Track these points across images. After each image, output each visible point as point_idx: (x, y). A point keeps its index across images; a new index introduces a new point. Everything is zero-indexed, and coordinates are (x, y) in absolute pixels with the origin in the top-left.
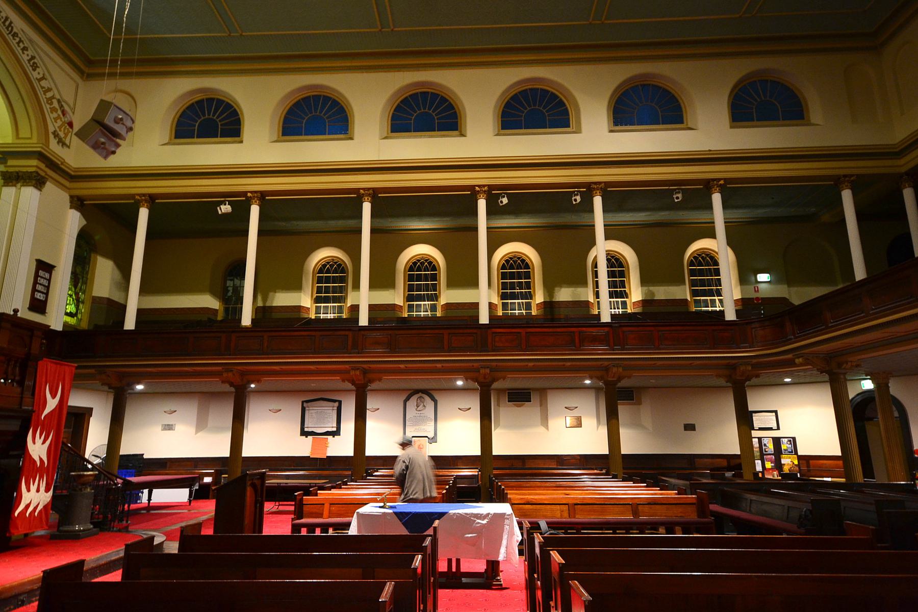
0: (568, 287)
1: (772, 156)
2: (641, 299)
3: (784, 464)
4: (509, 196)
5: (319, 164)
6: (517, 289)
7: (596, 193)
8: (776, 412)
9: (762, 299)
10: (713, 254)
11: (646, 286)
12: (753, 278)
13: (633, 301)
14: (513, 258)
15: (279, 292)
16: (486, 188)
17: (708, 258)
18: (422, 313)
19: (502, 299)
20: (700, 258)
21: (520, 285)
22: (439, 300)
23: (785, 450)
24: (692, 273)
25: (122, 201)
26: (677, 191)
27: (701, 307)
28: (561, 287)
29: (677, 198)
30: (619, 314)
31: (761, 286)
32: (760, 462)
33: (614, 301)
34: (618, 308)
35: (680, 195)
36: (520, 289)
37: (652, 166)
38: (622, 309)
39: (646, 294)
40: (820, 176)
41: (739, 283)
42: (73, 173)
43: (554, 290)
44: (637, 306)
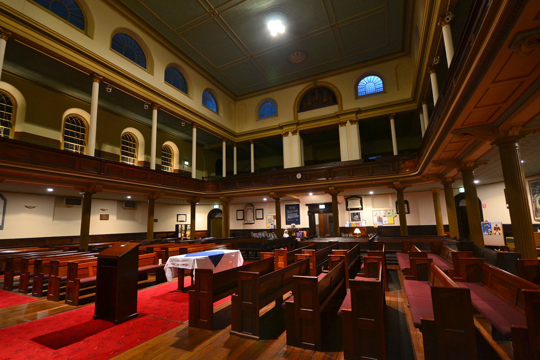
0: (110, 145)
1: (31, 25)
2: (143, 160)
3: (187, 234)
4: (113, 88)
5: (31, 20)
6: (76, 137)
7: (96, 80)
8: (186, 215)
9: (185, 171)
10: (9, 96)
11: (147, 155)
12: (183, 163)
13: (138, 160)
14: (75, 118)
15: (108, 145)
16: (197, 125)
17: (79, 121)
18: (74, 151)
19: (64, 140)
20: (74, 119)
21: (78, 135)
22: (13, 127)
23: (188, 229)
24: (67, 126)
25: (136, 97)
26: (146, 103)
27: (124, 161)
28: (106, 144)
29: (183, 124)
30: (131, 165)
31: (185, 166)
32: (180, 234)
33: (129, 158)
34: (131, 162)
35: (111, 89)
36: (78, 138)
37: (142, 88)
38: (75, 150)
39: (146, 159)
40: (208, 129)
41: (144, 154)
43: (102, 144)
44: (140, 163)
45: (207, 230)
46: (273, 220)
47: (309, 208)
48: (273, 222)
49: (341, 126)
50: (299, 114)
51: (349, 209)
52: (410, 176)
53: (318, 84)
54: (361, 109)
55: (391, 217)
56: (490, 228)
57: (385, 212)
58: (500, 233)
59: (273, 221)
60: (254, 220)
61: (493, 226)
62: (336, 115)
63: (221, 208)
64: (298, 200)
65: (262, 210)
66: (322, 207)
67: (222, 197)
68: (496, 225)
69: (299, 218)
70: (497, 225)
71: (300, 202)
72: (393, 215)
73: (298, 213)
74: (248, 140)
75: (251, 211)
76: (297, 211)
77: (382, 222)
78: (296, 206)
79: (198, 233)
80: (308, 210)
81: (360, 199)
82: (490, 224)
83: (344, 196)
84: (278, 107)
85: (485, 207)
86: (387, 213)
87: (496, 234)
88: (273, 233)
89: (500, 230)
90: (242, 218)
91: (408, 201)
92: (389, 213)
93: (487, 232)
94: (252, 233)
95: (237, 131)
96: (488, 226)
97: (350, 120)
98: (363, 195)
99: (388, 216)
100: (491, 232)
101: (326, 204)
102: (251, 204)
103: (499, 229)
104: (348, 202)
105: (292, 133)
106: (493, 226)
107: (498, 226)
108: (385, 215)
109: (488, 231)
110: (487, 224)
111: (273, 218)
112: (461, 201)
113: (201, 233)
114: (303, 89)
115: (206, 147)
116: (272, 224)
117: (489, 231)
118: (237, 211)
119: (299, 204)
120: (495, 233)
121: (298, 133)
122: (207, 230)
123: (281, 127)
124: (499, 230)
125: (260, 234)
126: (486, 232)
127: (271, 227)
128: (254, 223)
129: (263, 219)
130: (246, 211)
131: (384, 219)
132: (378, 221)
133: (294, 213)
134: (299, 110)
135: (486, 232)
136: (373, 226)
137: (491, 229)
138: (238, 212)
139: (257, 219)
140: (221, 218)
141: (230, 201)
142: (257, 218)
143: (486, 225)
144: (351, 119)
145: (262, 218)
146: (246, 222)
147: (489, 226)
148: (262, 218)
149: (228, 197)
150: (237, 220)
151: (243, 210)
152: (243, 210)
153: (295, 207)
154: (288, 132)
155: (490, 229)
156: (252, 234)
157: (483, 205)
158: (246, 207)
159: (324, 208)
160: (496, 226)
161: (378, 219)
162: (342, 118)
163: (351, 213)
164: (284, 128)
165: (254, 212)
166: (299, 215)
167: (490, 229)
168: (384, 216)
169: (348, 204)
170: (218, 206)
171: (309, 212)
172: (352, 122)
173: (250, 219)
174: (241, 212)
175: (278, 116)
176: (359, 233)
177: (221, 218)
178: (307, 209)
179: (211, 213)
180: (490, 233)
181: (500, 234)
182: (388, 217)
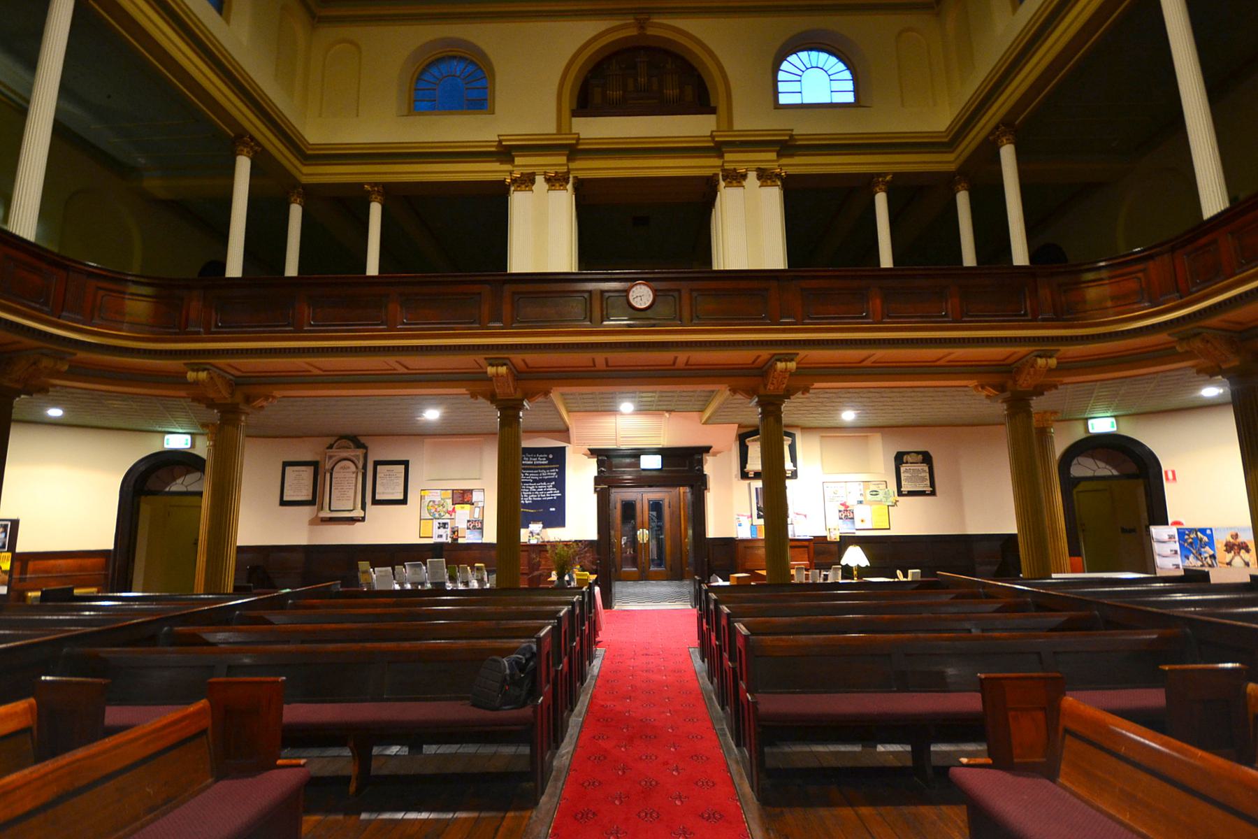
42: (946, 140)
45: (111, 546)
46: (450, 508)
47: (600, 464)
48: (447, 516)
49: (729, 185)
50: (574, 119)
51: (751, 475)
52: (1122, 332)
53: (651, 31)
54: (796, 140)
55: (883, 507)
56: (1211, 543)
57: (861, 487)
58: (1247, 560)
59: (449, 512)
60: (363, 508)
61: (1221, 539)
62: (712, 144)
63: (203, 449)
64: (564, 433)
65: (402, 467)
66: (651, 462)
67: (203, 375)
68: (1236, 536)
69: (560, 503)
70: (1237, 535)
71: (569, 443)
72: (887, 498)
73: (560, 484)
74: (361, 185)
75: (353, 468)
76: (554, 475)
77: (853, 523)
78: (551, 456)
79: (52, 562)
80: (596, 474)
81: (790, 439)
82: (1208, 532)
83: (740, 426)
84: (497, 80)
85: (1174, 478)
86: (868, 492)
87: (1233, 563)
88: (479, 569)
89: (1248, 551)
90: (310, 498)
91: (931, 453)
92: (875, 493)
93: (1197, 559)
94: (364, 565)
95: (315, 134)
96: (1201, 540)
97: (758, 170)
98: (796, 427)
99: (871, 503)
100: (1213, 557)
101: (665, 453)
102: (355, 441)
103: (1244, 547)
104: (747, 447)
105: (548, 180)
106: (1221, 539)
107: (1240, 539)
108: (861, 498)
109: (1200, 554)
110: (1199, 534)
111: (450, 501)
112: (1075, 461)
113: (70, 562)
114: (595, 39)
115: (155, 184)
116: (444, 525)
117: (1207, 555)
118: (286, 464)
119: (563, 449)
120: (1228, 560)
121: (570, 186)
122: (111, 546)
123: (505, 153)
124: (1243, 551)
125: (407, 571)
126: (1191, 557)
127: (441, 536)
128: (363, 519)
129: (404, 502)
130: (328, 466)
131: (860, 512)
132: (841, 518)
133: (543, 480)
134: (574, 107)
135: (1191, 557)
136: (826, 537)
137: (1213, 549)
138: (288, 469)
139: (375, 502)
140: (200, 494)
141: (248, 400)
142: (378, 497)
143: (1192, 536)
144: (763, 166)
145: (401, 497)
146: (326, 514)
147: (1205, 539)
148: (401, 497)
149: (239, 382)
150: (283, 503)
151: (315, 465)
152: (315, 465)
153: (548, 459)
154: (534, 174)
155: (1207, 548)
156: (366, 572)
157: (1166, 472)
158: (330, 452)
159: (660, 467)
160: (1232, 540)
161: (840, 511)
162: (733, 159)
163: (757, 489)
164: (516, 159)
165: (369, 473)
166: (563, 491)
167: (1207, 548)
168: (861, 502)
169: (749, 455)
170: (188, 437)
171: (598, 480)
172: (765, 177)
173: (344, 498)
174: (307, 473)
175: (493, 113)
176: (867, 566)
177: (200, 494)
178: (591, 468)
179: (142, 468)
180: (1208, 560)
181: (1247, 564)
182: (871, 505)
